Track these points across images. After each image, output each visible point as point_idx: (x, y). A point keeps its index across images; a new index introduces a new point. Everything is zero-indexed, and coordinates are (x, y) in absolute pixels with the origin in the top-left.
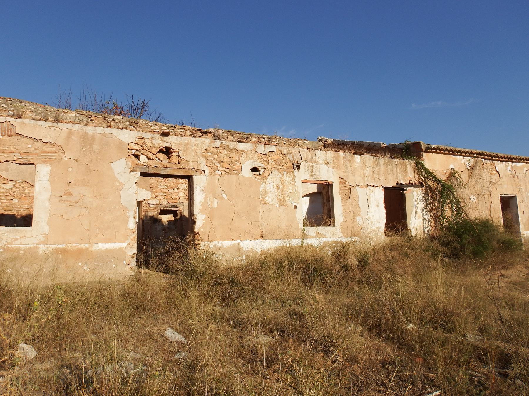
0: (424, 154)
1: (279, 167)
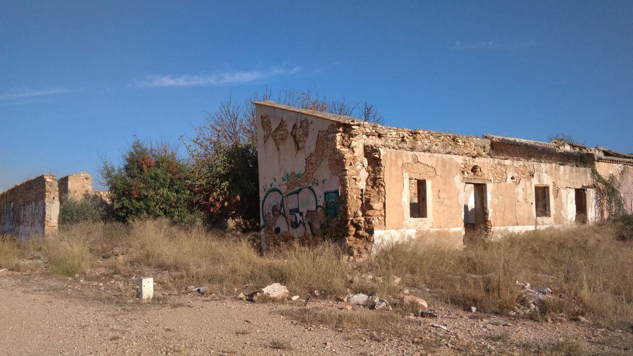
0: (596, 163)
1: (524, 176)
